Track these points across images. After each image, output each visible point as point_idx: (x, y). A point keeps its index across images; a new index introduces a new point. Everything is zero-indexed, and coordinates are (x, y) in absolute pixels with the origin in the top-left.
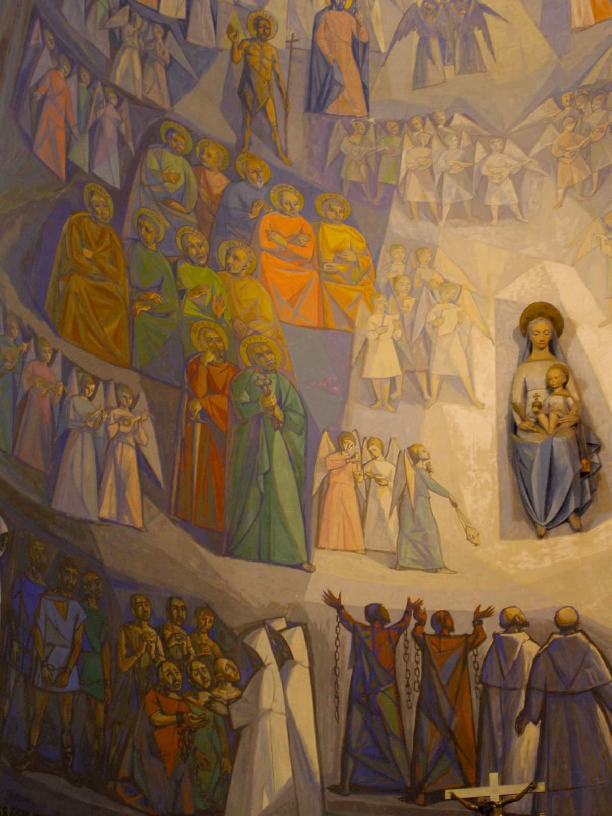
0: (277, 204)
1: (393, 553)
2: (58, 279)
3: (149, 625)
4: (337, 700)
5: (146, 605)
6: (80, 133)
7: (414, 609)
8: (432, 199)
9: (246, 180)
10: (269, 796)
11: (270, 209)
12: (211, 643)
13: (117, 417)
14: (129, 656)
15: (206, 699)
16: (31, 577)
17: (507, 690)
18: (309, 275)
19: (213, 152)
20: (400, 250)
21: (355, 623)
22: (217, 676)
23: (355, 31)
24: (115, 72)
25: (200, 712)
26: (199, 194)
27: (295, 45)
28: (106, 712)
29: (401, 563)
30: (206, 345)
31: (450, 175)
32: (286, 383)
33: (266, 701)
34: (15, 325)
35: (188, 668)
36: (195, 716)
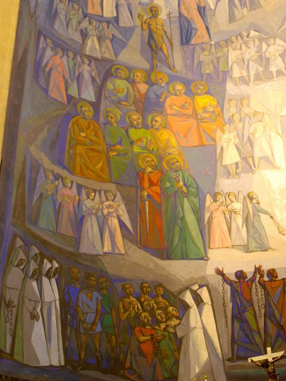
0: (173, 92)
1: (246, 245)
2: (70, 149)
3: (133, 297)
4: (226, 318)
5: (131, 288)
6: (72, 81)
7: (258, 270)
8: (245, 74)
9: (157, 84)
10: (199, 366)
11: (170, 95)
12: (164, 301)
13: (107, 206)
14: (124, 312)
15: (164, 326)
16: (73, 285)
18: (192, 122)
19: (139, 75)
20: (233, 101)
21: (231, 281)
22: (168, 315)
23: (198, 3)
24: (86, 48)
25: (161, 333)
26: (135, 96)
27: (171, 15)
28: (116, 340)
29: (250, 250)
30: (146, 164)
31: (252, 61)
32: (186, 175)
33: (193, 323)
34: (50, 174)
35: (154, 314)
36: (159, 335)
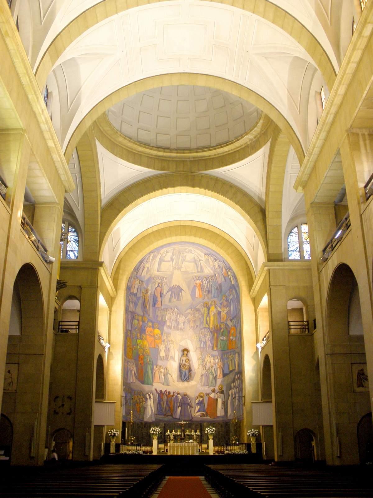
7: (166, 391)
8: (171, 325)
17: (177, 403)
18: (153, 338)
19: (140, 317)
27: (152, 294)
